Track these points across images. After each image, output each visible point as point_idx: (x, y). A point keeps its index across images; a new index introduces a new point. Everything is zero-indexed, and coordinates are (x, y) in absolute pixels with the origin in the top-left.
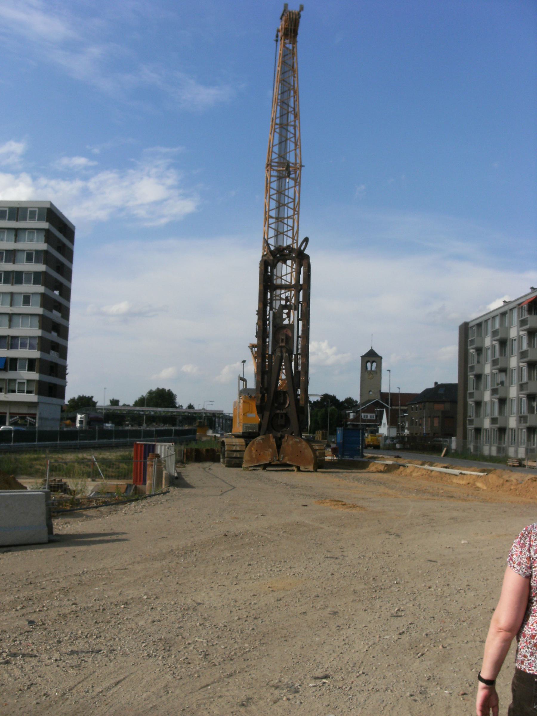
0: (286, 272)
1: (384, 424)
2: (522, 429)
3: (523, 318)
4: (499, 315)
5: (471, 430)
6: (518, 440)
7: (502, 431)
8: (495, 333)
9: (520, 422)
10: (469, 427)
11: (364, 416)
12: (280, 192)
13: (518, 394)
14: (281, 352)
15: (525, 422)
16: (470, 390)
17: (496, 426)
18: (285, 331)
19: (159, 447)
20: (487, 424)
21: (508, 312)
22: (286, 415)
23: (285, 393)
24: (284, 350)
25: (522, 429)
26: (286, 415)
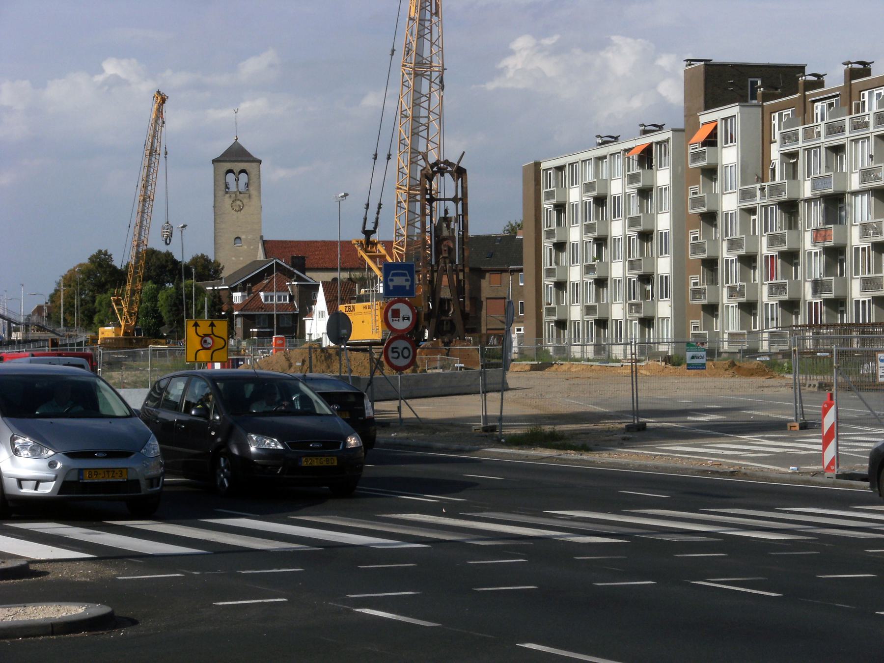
0: (446, 186)
1: (322, 314)
2: (631, 321)
3: (631, 172)
4: (593, 160)
5: (549, 323)
6: (627, 335)
7: (602, 323)
8: (589, 187)
9: (630, 312)
10: (545, 319)
11: (266, 298)
12: (417, 92)
13: (581, 237)
14: (445, 263)
15: (638, 312)
16: (546, 264)
17: (593, 317)
18: (445, 243)
19: (670, 337)
20: (576, 313)
21: (608, 157)
22: (451, 321)
23: (449, 300)
24: (447, 261)
25: (631, 321)
26: (451, 321)
